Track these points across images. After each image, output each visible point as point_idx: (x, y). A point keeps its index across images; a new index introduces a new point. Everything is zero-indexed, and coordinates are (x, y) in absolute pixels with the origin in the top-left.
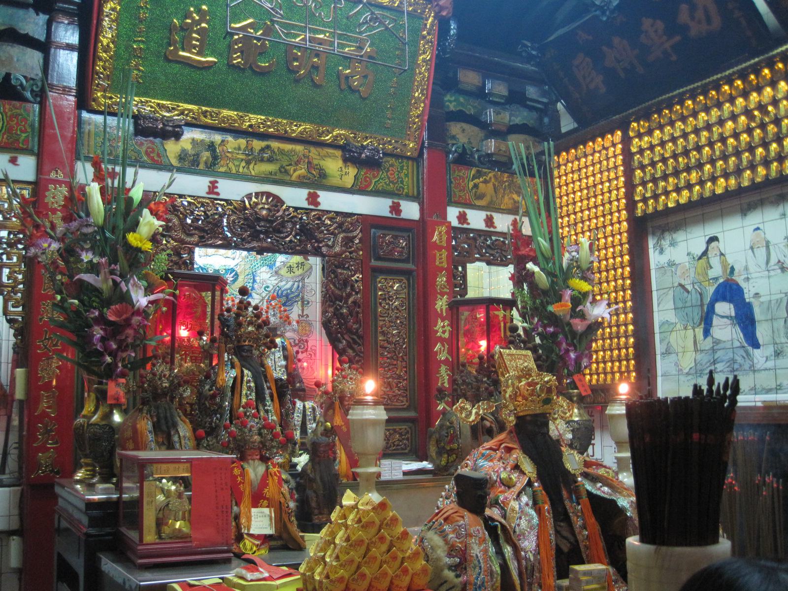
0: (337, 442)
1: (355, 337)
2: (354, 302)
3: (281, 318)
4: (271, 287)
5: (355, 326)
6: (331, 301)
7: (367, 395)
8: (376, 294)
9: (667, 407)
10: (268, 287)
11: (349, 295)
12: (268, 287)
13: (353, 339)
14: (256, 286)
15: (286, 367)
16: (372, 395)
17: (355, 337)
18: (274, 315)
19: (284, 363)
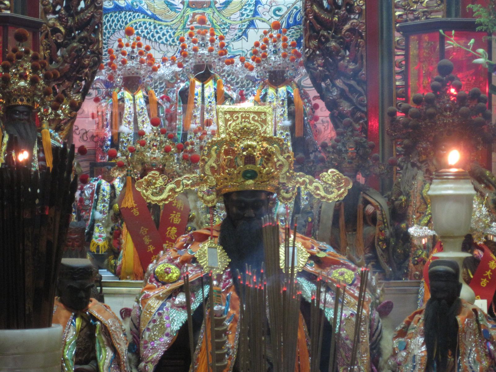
0: (125, 230)
1: (352, 82)
2: (352, 30)
3: (285, 56)
4: (284, 9)
5: (352, 66)
6: (314, 31)
7: (451, 167)
8: (390, 14)
9: (30, 175)
10: (279, 10)
11: (344, 20)
12: (279, 10)
13: (350, 86)
14: (260, 9)
15: (292, 129)
16: (456, 166)
17: (352, 82)
18: (275, 53)
19: (288, 123)
